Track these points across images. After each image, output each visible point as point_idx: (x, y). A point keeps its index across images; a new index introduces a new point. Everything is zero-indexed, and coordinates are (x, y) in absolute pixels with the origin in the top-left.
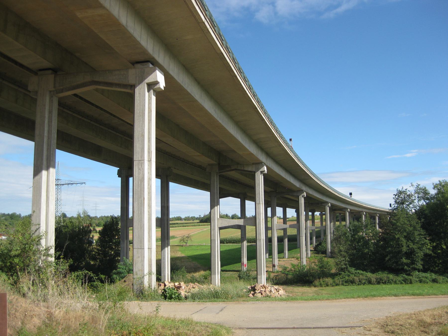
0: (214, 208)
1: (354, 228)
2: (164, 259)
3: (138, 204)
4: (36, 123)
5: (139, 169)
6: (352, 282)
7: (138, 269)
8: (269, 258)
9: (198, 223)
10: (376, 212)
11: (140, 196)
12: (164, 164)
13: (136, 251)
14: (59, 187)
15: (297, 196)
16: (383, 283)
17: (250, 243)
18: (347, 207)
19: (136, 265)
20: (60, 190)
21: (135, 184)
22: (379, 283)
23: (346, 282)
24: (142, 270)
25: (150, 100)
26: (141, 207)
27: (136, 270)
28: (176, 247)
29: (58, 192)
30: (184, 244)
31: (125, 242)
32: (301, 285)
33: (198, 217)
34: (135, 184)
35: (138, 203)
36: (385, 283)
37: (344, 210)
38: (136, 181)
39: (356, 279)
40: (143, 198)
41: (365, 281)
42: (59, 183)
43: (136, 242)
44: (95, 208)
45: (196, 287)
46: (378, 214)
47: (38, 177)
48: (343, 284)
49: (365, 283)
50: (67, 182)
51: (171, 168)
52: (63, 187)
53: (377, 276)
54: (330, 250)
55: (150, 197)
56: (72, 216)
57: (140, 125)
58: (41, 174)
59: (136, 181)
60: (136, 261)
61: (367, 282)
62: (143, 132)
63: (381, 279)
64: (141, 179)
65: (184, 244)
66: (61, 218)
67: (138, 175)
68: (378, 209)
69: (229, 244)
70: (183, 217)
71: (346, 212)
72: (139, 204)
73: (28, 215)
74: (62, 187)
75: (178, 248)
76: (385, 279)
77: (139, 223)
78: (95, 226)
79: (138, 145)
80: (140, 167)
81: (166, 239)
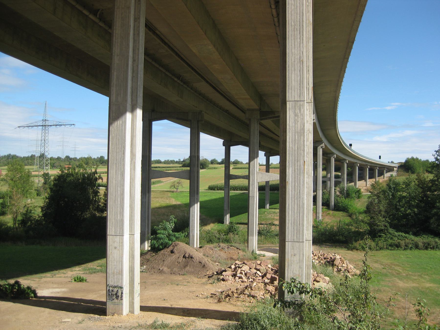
0: (254, 160)
1: (394, 186)
2: (193, 217)
3: (295, 171)
4: (114, 35)
5: (296, 115)
6: (398, 246)
7: (293, 275)
8: (269, 208)
9: (180, 167)
10: (367, 164)
11: (298, 158)
12: (197, 107)
13: (290, 245)
14: (47, 128)
15: (316, 147)
16: (431, 248)
17: (242, 190)
18: (346, 159)
19: (289, 267)
20: (47, 131)
21: (289, 138)
22: (426, 248)
23: (390, 245)
24: (300, 275)
25: (309, 7)
26: (299, 176)
27: (289, 275)
28: (166, 192)
29: (46, 133)
30: (175, 190)
31: (147, 196)
32: (332, 245)
33: (178, 160)
34: (289, 138)
35: (293, 169)
36: (433, 248)
37: (342, 161)
38: (291, 133)
39: (403, 243)
40: (302, 162)
41: (412, 246)
42: (47, 123)
43: (290, 231)
44: (74, 149)
45: (320, 280)
46: (369, 165)
47: (119, 122)
48: (387, 248)
49: (411, 248)
50: (55, 123)
51: (203, 112)
52: (50, 128)
53: (425, 241)
54: (333, 204)
55: (310, 160)
56: (51, 157)
57: (296, 44)
58: (123, 117)
59: (291, 133)
60: (290, 262)
61: (414, 247)
62: (301, 55)
63: (429, 244)
64: (299, 131)
65: (175, 190)
66: (49, 161)
67: (294, 124)
68: (370, 161)
69: (220, 191)
70: (163, 160)
71: (344, 163)
72: (296, 170)
73: (8, 155)
74: (49, 128)
75: (170, 194)
76: (434, 243)
77: (296, 201)
78: (76, 167)
79: (293, 75)
80: (297, 111)
81: (196, 194)
